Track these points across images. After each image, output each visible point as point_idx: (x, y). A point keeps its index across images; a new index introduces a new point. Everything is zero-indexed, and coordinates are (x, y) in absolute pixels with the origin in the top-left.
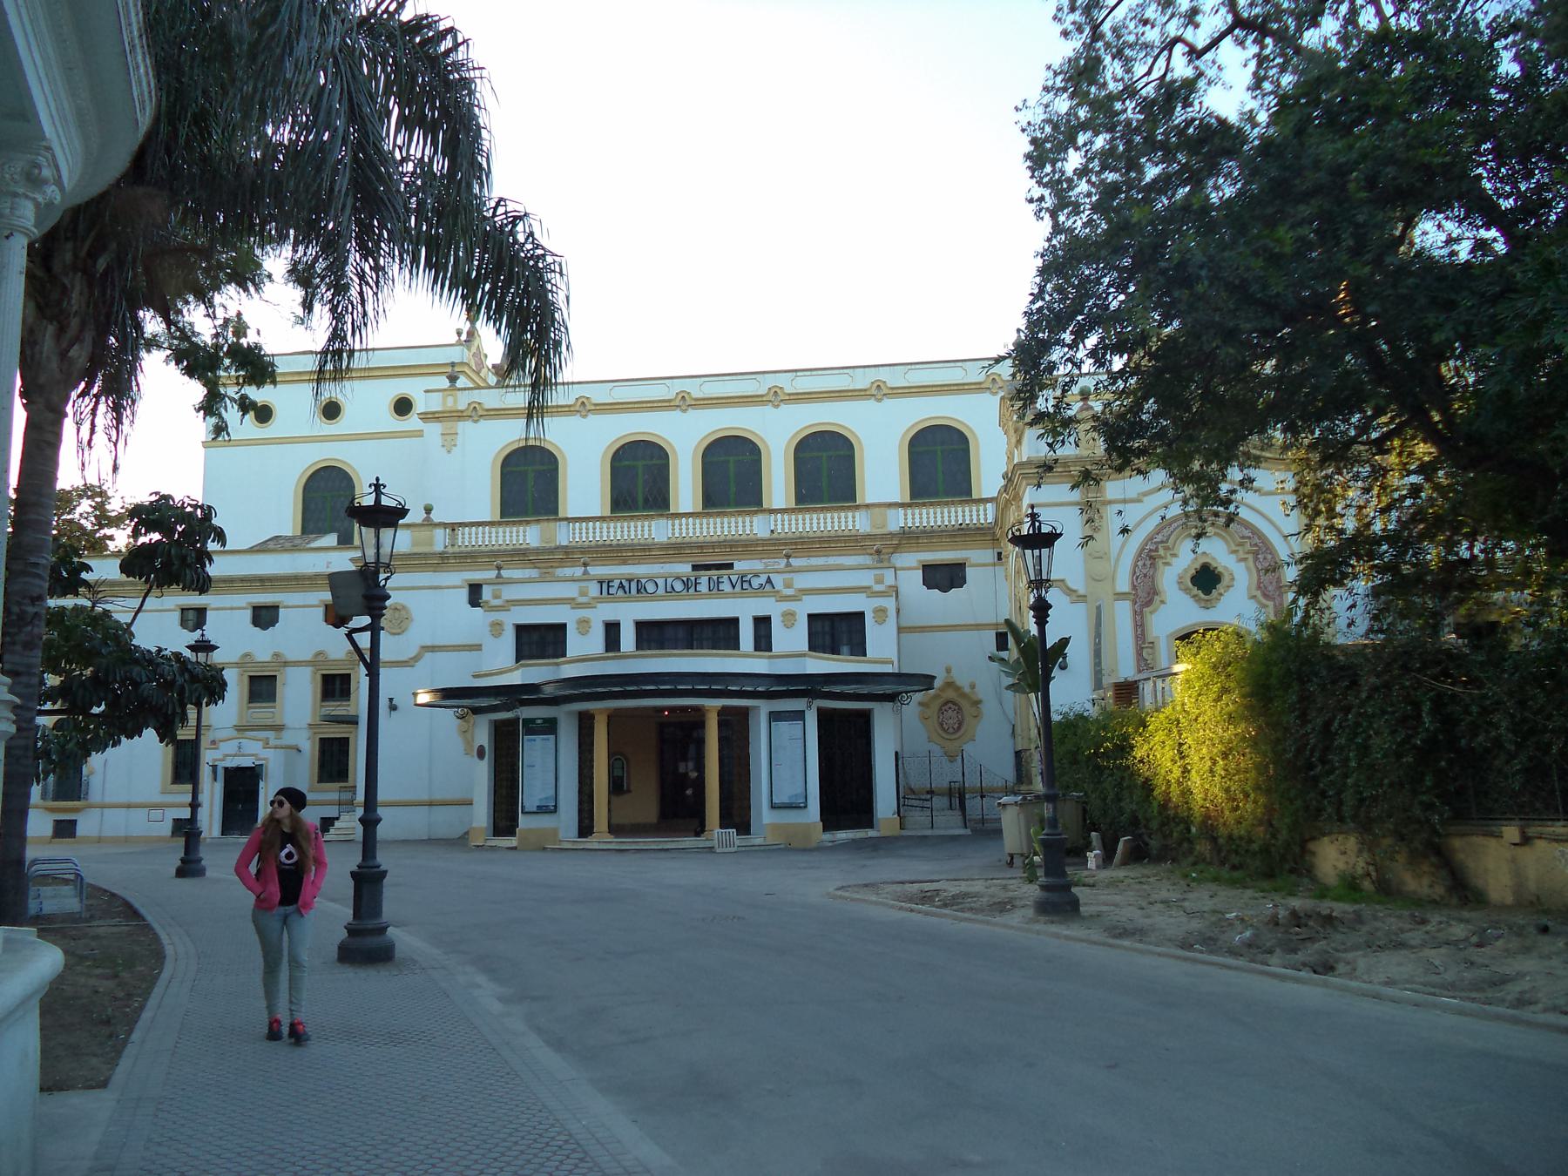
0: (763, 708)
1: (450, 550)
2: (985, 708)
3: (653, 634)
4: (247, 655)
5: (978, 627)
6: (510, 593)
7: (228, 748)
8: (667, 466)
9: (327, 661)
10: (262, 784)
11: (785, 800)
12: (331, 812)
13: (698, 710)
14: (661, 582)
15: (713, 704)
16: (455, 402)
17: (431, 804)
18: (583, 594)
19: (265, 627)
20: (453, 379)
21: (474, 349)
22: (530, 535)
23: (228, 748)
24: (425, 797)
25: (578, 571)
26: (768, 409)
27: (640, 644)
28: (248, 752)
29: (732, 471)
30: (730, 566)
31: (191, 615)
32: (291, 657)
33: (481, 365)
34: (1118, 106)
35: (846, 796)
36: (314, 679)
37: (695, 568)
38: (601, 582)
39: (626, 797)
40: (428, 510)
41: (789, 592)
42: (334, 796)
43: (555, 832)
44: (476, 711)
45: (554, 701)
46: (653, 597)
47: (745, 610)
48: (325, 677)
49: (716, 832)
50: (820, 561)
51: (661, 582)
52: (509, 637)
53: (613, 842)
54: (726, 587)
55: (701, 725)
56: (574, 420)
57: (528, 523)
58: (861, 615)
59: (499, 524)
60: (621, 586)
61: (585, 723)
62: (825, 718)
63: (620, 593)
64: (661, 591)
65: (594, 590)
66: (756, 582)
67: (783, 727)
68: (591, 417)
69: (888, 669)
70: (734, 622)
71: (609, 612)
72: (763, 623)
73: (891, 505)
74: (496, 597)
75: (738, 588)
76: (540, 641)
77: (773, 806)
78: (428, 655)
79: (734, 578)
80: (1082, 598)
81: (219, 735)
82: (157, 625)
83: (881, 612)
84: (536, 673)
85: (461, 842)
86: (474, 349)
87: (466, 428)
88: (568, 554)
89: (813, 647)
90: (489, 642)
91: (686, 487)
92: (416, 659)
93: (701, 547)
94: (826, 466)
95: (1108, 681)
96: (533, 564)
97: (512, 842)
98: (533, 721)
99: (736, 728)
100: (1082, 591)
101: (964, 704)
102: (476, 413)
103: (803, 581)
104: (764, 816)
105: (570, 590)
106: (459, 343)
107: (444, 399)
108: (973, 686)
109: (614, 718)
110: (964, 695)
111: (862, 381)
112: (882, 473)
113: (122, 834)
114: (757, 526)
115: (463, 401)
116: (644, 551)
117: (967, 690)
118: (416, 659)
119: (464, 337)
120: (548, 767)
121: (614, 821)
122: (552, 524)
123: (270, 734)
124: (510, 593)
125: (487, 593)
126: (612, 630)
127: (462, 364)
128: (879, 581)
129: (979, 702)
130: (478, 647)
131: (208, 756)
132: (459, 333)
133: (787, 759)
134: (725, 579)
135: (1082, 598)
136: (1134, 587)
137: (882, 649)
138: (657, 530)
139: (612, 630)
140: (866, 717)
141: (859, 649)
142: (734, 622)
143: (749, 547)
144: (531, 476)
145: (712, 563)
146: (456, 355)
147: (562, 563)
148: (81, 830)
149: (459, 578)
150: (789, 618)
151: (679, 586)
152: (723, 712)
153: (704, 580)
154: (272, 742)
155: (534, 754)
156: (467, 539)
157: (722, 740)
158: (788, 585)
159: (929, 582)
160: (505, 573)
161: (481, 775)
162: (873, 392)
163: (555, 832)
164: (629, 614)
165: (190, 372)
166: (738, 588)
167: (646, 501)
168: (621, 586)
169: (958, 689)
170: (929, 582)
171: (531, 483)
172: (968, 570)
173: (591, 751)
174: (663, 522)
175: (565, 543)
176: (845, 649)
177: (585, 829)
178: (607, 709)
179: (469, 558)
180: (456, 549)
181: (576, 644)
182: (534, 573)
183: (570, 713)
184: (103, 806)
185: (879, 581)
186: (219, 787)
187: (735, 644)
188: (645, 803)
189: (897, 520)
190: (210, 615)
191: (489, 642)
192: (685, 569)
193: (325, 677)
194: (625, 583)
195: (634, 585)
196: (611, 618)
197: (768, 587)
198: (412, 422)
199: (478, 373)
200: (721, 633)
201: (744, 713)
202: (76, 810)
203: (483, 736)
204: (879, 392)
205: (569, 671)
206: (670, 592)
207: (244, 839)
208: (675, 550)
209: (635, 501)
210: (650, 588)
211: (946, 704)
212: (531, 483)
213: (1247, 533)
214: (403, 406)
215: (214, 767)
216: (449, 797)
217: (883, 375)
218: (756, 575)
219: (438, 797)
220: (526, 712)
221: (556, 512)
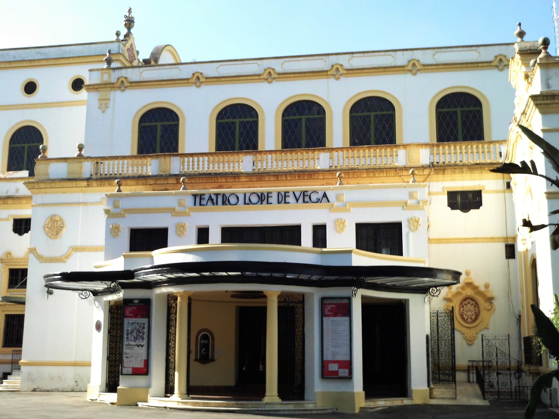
0: (314, 296)
2: (420, 222)
3: (231, 234)
5: (492, 240)
13: (260, 295)
15: (273, 291)
16: (110, 77)
19: (21, 234)
20: (109, 61)
22: (151, 166)
29: (304, 125)
34: (115, 331)
38: (121, 191)
39: (211, 365)
40: (81, 148)
42: (9, 357)
47: (305, 218)
53: (190, 403)
55: (263, 311)
60: (210, 198)
63: (210, 203)
68: (343, 80)
73: (124, 157)
76: (148, 239)
79: (297, 194)
84: (364, 259)
86: (128, 46)
87: (117, 96)
91: (270, 133)
94: (374, 122)
95: (522, 336)
99: (292, 312)
102: (124, 85)
106: (118, 41)
107: (102, 75)
108: (487, 286)
111: (401, 59)
112: (197, 133)
114: (321, 160)
115: (114, 76)
117: (482, 289)
118: (67, 256)
119: (121, 37)
121: (192, 384)
129: (108, 107)
132: (118, 34)
134: (291, 194)
137: (414, 254)
138: (244, 163)
139: (203, 235)
140: (223, 241)
141: (398, 250)
144: (372, 117)
146: (114, 48)
151: (254, 199)
156: (107, 168)
159: (453, 205)
164: (217, 219)
165: (152, 54)
166: (301, 200)
168: (210, 198)
169: (475, 288)
170: (453, 205)
171: (159, 134)
172: (484, 195)
176: (384, 250)
187: (298, 242)
188: (224, 369)
189: (205, 166)
194: (214, 197)
196: (319, 221)
198: (83, 94)
200: (289, 235)
201: (302, 299)
204: (414, 68)
207: (19, 378)
209: (14, 143)
210: (233, 200)
211: (465, 299)
212: (159, 134)
213: (474, 303)
214: (77, 85)
217: (418, 55)
221: (176, 149)
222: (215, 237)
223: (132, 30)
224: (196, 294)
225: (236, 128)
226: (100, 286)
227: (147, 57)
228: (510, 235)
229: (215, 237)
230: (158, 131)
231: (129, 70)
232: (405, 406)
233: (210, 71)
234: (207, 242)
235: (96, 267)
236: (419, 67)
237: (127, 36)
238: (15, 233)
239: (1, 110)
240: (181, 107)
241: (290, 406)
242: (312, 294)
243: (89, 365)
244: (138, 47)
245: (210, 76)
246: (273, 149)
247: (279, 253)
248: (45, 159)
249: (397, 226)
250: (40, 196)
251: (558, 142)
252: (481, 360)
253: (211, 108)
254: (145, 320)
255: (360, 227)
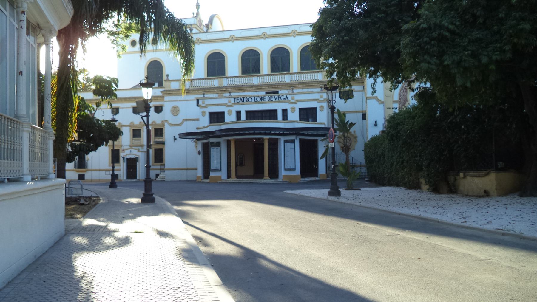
0: (282, 139)
1: (191, 88)
2: (358, 139)
3: (252, 115)
4: (132, 122)
5: (357, 112)
6: (208, 102)
7: (127, 152)
8: (224, 60)
9: (156, 124)
10: (138, 163)
11: (289, 168)
12: (158, 172)
13: (262, 139)
14: (253, 98)
17: (187, 169)
18: (229, 102)
21: (198, 19)
22: (215, 83)
23: (127, 152)
24: (185, 167)
25: (227, 95)
26: (292, 38)
27: (247, 118)
28: (134, 153)
30: (277, 92)
31: (115, 110)
32: (123, 124)
33: (201, 24)
35: (308, 166)
36: (130, 131)
37: (267, 93)
38: (235, 98)
41: (293, 101)
42: (159, 167)
43: (220, 177)
44: (198, 140)
45: (219, 137)
46: (250, 103)
47: (279, 107)
48: (134, 130)
49: (267, 179)
50: (306, 90)
51: (253, 98)
52: (207, 117)
54: (273, 99)
55: (263, 144)
56: (230, 43)
57: (214, 79)
58: (315, 108)
59: (300, 73)
60: (241, 99)
61: (229, 142)
62: (301, 141)
63: (241, 102)
64: (253, 101)
65: (233, 101)
66: (282, 98)
67: (288, 145)
68: (235, 42)
69: (323, 126)
70: (275, 111)
71: (237, 108)
72: (285, 111)
73: (203, 79)
74: (293, 99)
75: (277, 100)
76: (217, 117)
77: (285, 170)
78: (185, 122)
79: (276, 97)
80: (383, 103)
81: (124, 148)
82: (103, 114)
83: (322, 108)
84: (215, 128)
85: (194, 182)
86: (198, 19)
88: (227, 89)
89: (301, 119)
90: (201, 118)
92: (182, 123)
93: (268, 86)
96: (216, 92)
97: (208, 180)
98: (213, 143)
100: (382, 100)
101: (352, 137)
103: (297, 97)
104: (282, 173)
105: (225, 101)
106: (194, 17)
108: (354, 132)
109: (236, 141)
110: (351, 135)
111: (227, 35)
112: (233, 66)
113: (98, 179)
114: (286, 79)
116: (250, 88)
117: (353, 133)
118: (182, 123)
119: (195, 15)
120: (219, 157)
122: (222, 79)
123: (140, 148)
124: (208, 102)
125: (200, 102)
126: (238, 113)
127: (194, 24)
128: (321, 97)
130: (198, 120)
131: (122, 155)
133: (290, 156)
134: (273, 97)
135: (383, 103)
136: (400, 99)
138: (255, 80)
139: (238, 113)
141: (315, 120)
142: (275, 111)
143: (283, 86)
145: (272, 91)
147: (225, 92)
148: (86, 178)
149: (193, 97)
150: (293, 109)
151: (259, 99)
152: (269, 140)
153: (267, 97)
154: (140, 150)
155: (214, 152)
157: (269, 149)
158: (293, 99)
160: (206, 96)
161: (199, 159)
162: (292, 34)
163: (220, 177)
164: (244, 108)
166: (277, 100)
167: (253, 70)
168: (241, 99)
173: (230, 152)
174: (256, 78)
175: (226, 85)
176: (310, 120)
177: (229, 176)
178: (234, 139)
179: (196, 90)
180: (193, 88)
181: (227, 118)
182: (216, 95)
183: (224, 140)
184: (92, 170)
185: (321, 97)
186: (125, 164)
188: (249, 169)
190: (120, 110)
191: (201, 118)
192: (263, 93)
193: (134, 130)
195: (245, 99)
196: (238, 110)
197: (286, 99)
199: (200, 27)
200: (271, 115)
202: (85, 171)
203: (200, 148)
205: (224, 127)
206: (256, 101)
208: (260, 87)
209: (279, 68)
210: (250, 100)
215: (124, 158)
216: (177, 167)
218: (283, 95)
219: (189, 167)
220: (212, 140)
221: (224, 74)
222: (243, 117)
223: (199, 10)
224: (238, 139)
225: (250, 62)
226: (200, 137)
227: (207, 23)
228: (364, 109)
229: (243, 117)
230: (216, 64)
231: (201, 34)
232: (316, 163)
233: (238, 35)
234: (277, 177)
235: (198, 129)
236: (266, 36)
237: (198, 14)
238: (320, 13)
239: (534, 240)
240: (288, 45)
241: (273, 180)
242: (120, 166)
243: (196, 169)
244: (202, 19)
245: (173, 123)
246: (296, 71)
247: (270, 123)
248: (168, 80)
249: (315, 109)
250: (167, 97)
251: (60, 15)
252: (361, 92)
253: (301, 44)
254: (68, 196)
255: (300, 109)
